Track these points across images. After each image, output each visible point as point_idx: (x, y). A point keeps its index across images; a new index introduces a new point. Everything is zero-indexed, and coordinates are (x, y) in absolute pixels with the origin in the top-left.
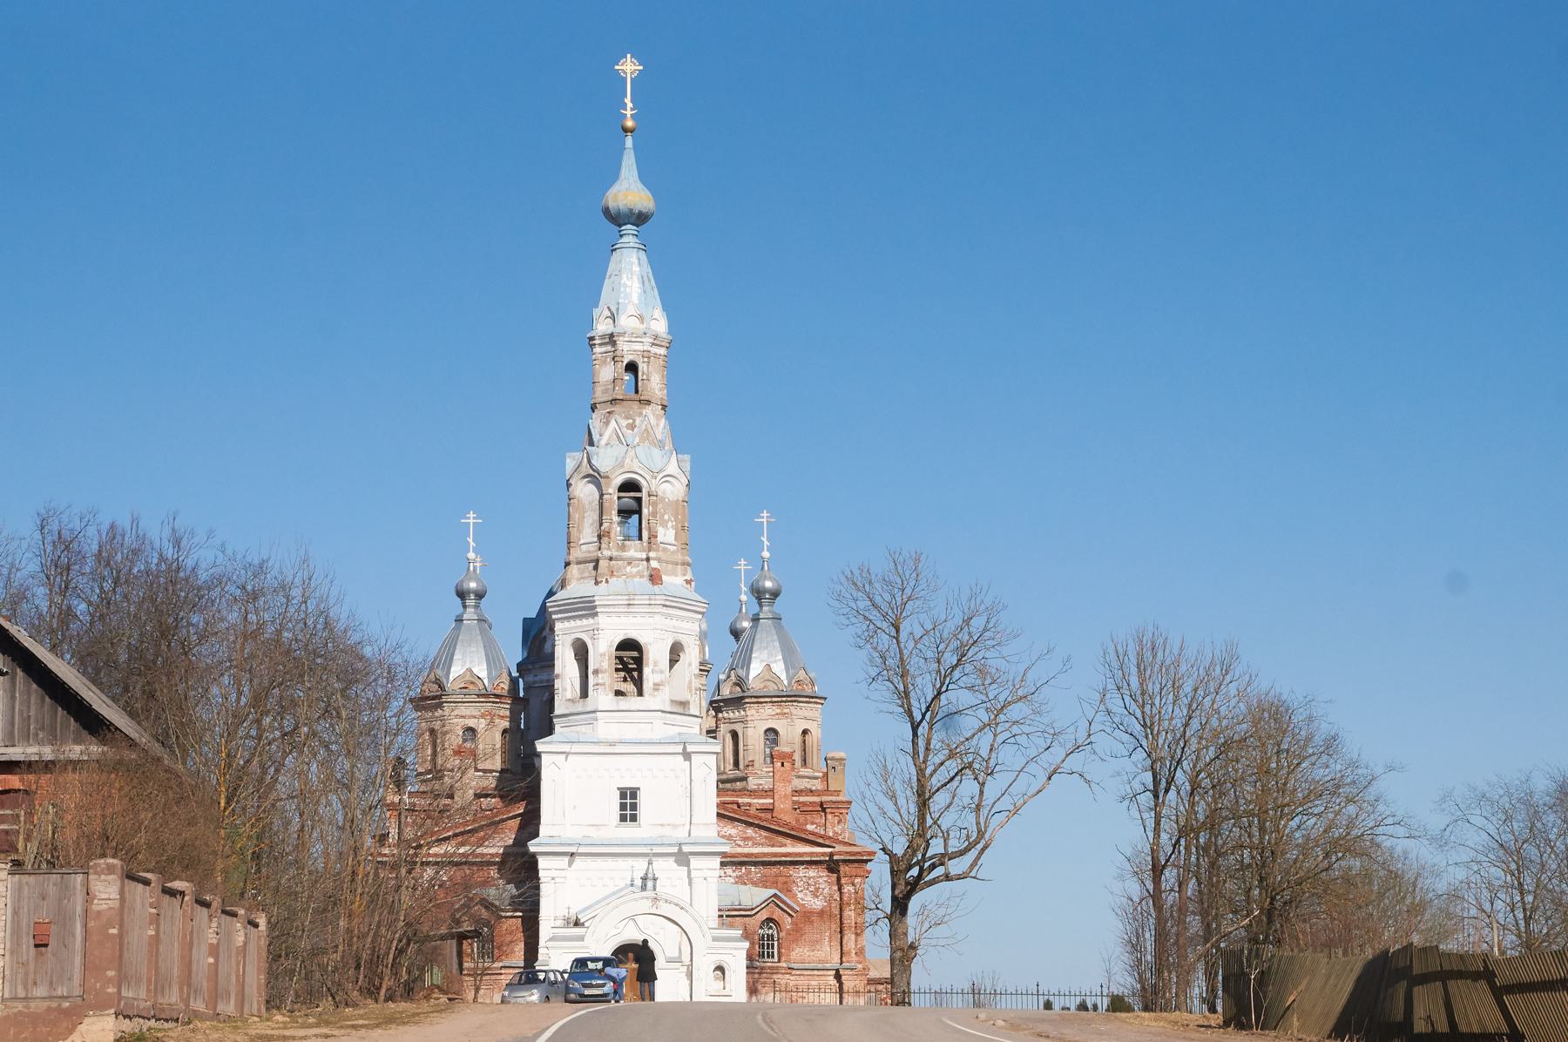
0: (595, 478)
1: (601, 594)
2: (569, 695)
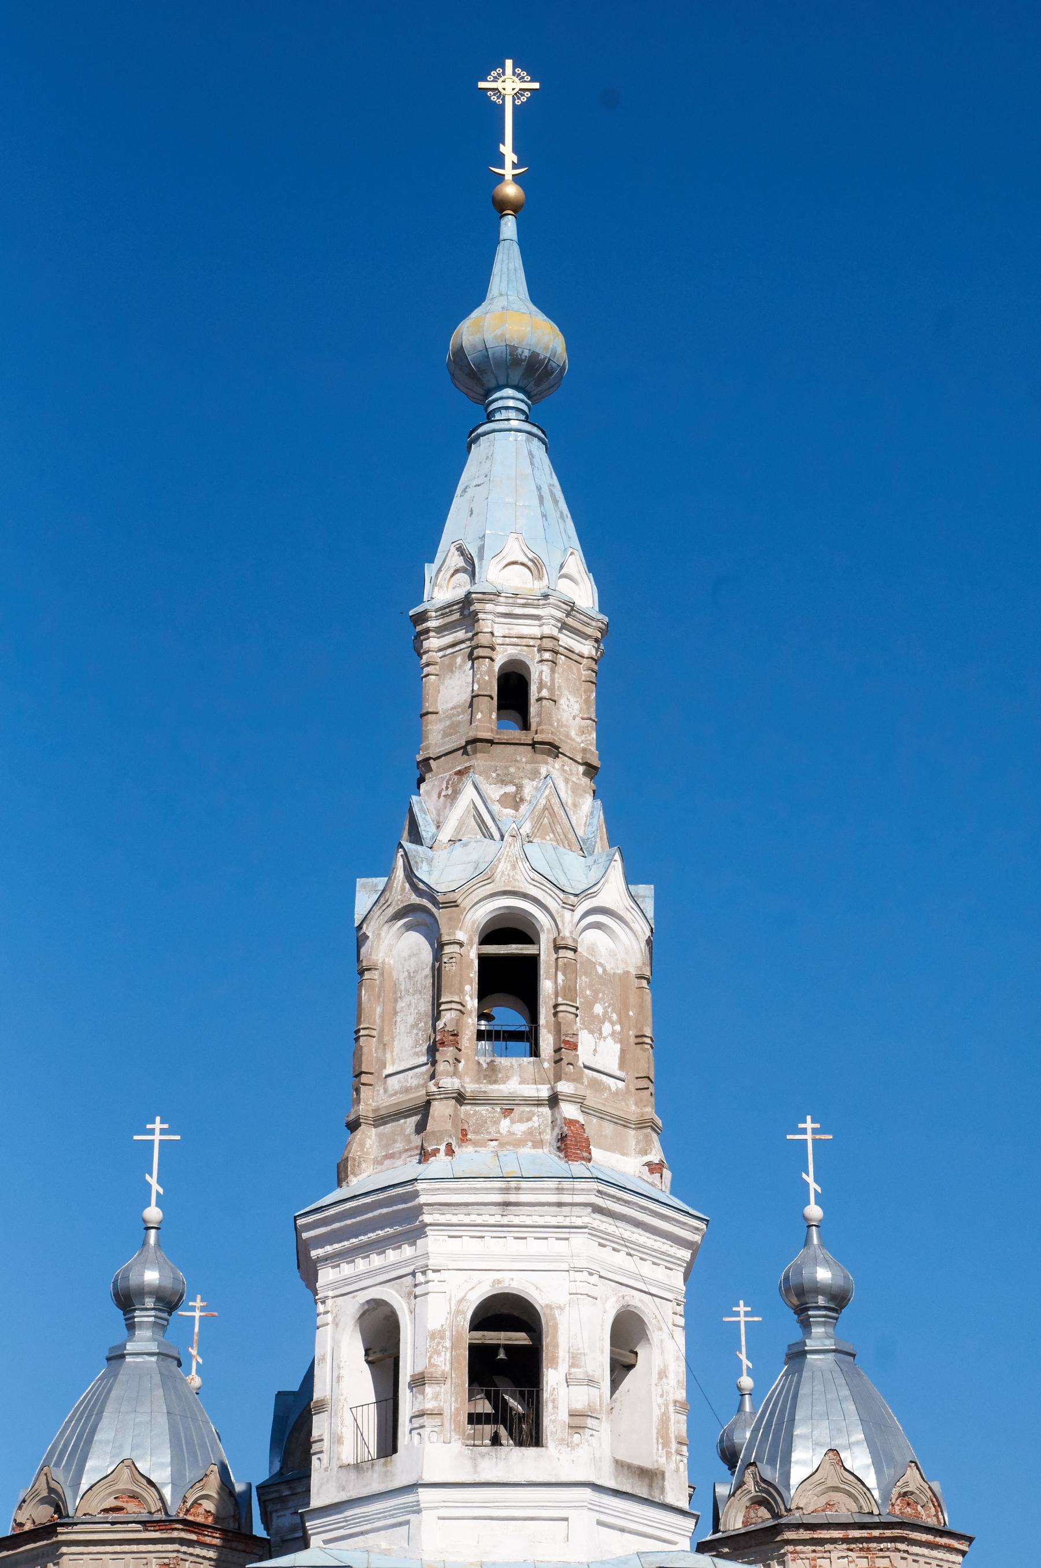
0: (424, 913)
1: (437, 1179)
2: (347, 1454)
